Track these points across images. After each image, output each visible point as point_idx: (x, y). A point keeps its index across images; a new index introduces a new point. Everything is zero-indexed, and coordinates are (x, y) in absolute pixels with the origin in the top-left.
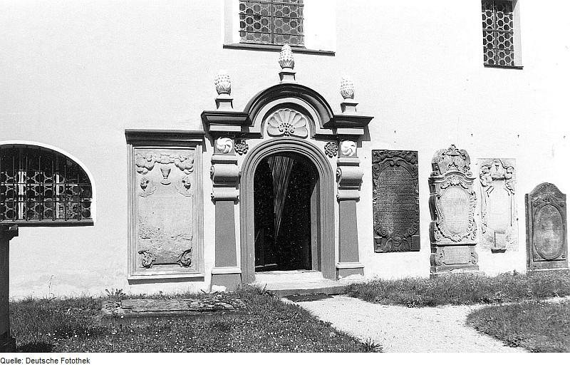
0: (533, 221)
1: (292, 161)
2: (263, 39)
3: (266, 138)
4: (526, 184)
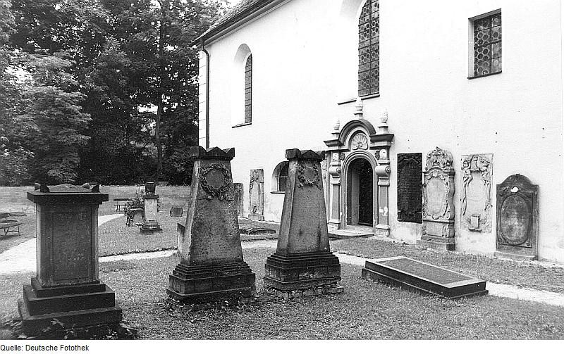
1: (202, 143)
3: (352, 151)
4: (499, 177)
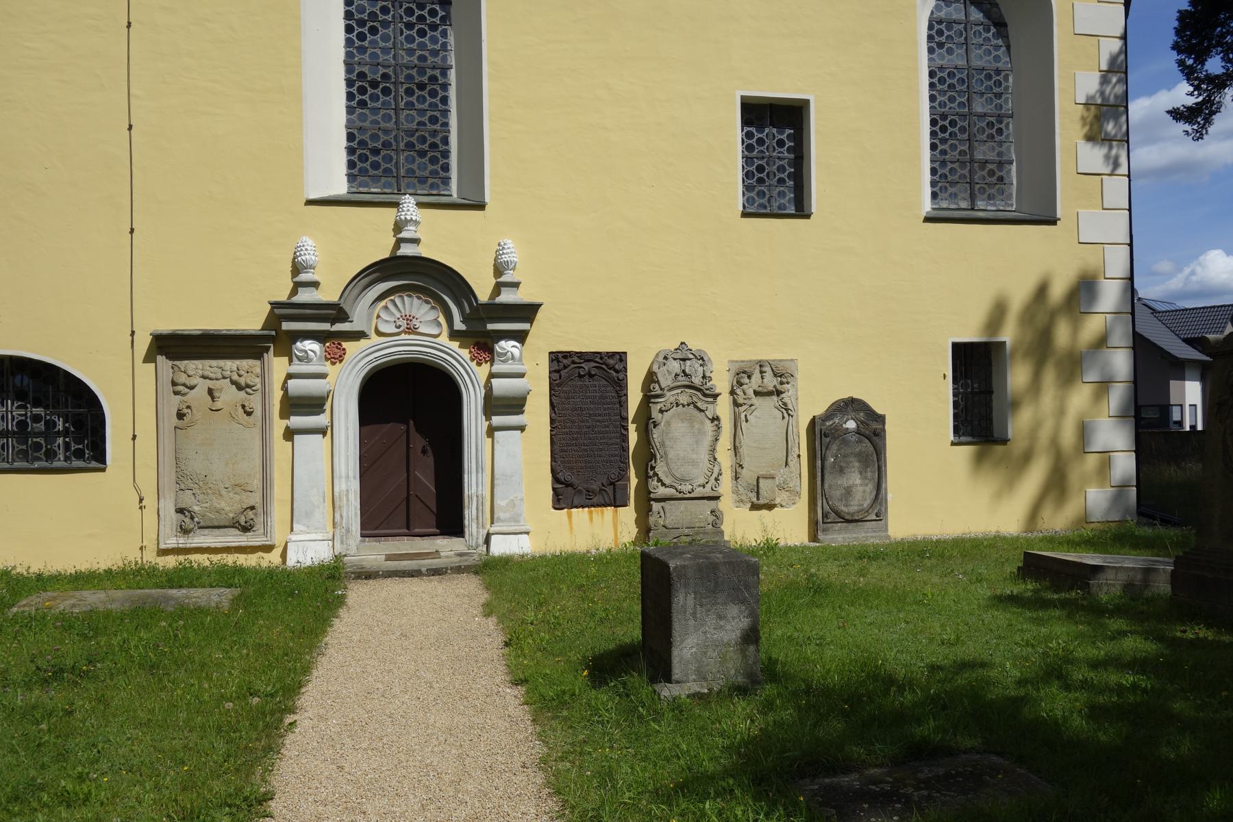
0: (823, 460)
2: (384, 186)
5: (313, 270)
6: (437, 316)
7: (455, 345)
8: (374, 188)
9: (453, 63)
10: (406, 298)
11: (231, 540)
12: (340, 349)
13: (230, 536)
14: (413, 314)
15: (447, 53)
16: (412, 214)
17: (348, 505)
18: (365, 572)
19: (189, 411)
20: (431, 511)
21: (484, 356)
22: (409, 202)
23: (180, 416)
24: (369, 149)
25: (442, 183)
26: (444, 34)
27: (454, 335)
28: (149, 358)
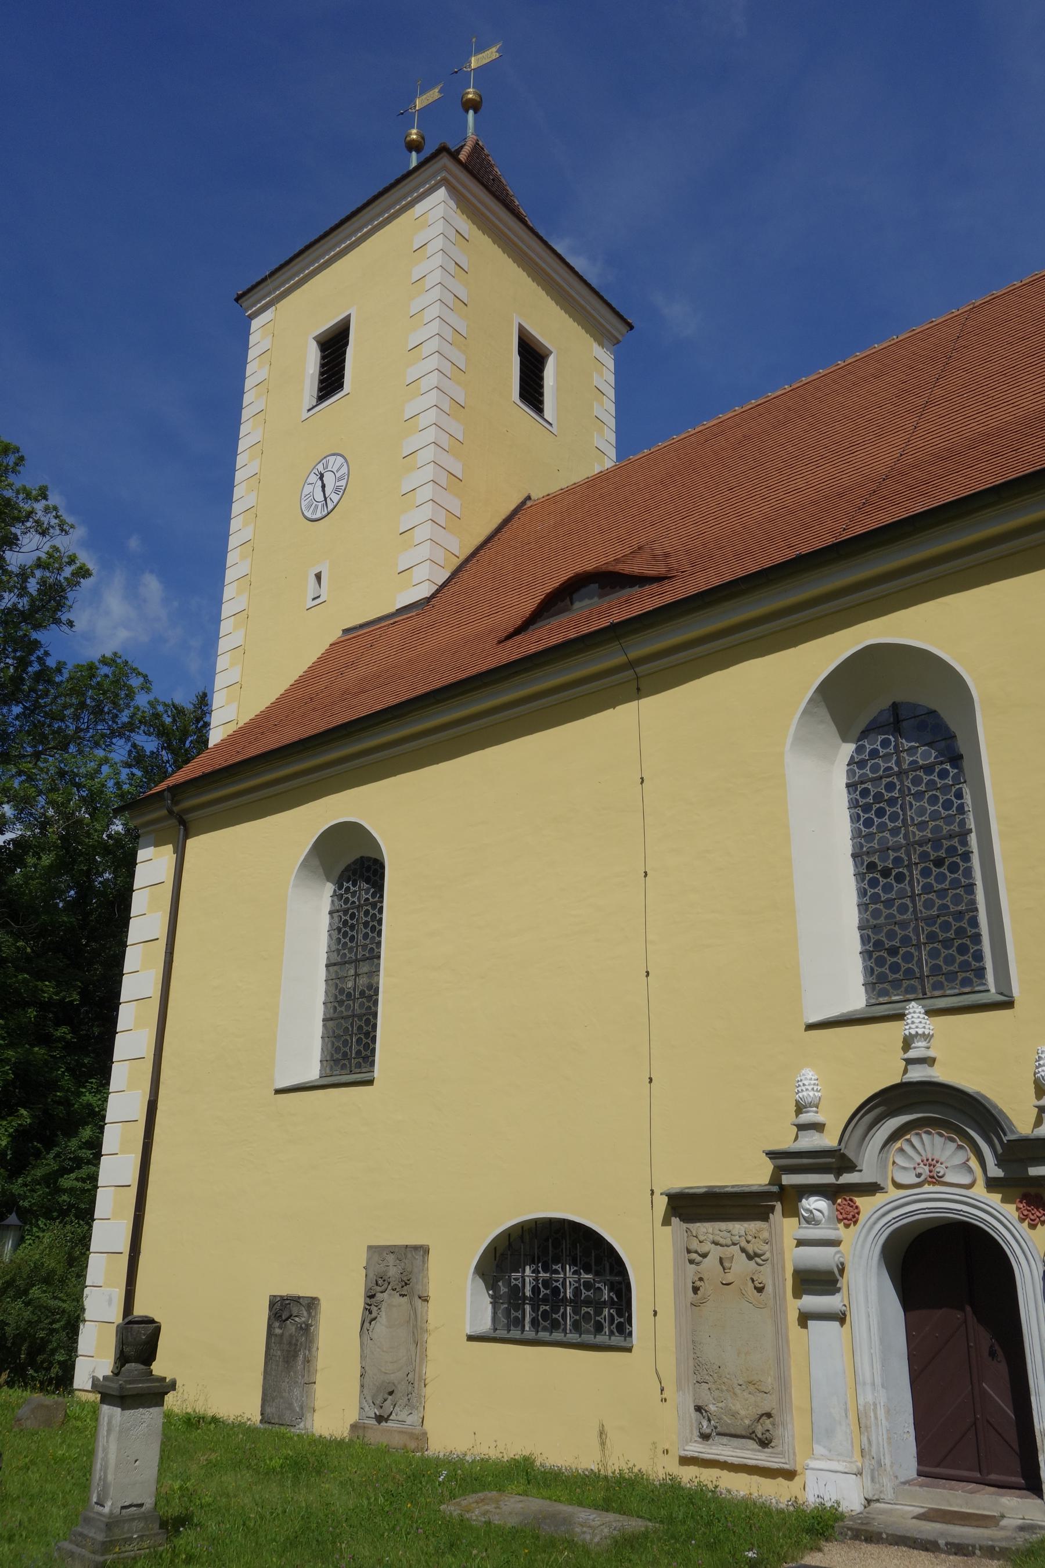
5: (814, 1109)
6: (966, 1159)
7: (995, 1199)
8: (895, 995)
9: (973, 826)
10: (924, 1136)
11: (760, 1457)
12: (852, 1207)
13: (748, 1450)
14: (936, 1157)
15: (965, 816)
16: (917, 1027)
17: (877, 1425)
18: (866, 1531)
19: (702, 1283)
20: (1014, 1451)
21: (1038, 1214)
22: (915, 1011)
23: (696, 1290)
24: (886, 949)
25: (976, 976)
26: (959, 795)
27: (992, 1184)
28: (666, 1222)
